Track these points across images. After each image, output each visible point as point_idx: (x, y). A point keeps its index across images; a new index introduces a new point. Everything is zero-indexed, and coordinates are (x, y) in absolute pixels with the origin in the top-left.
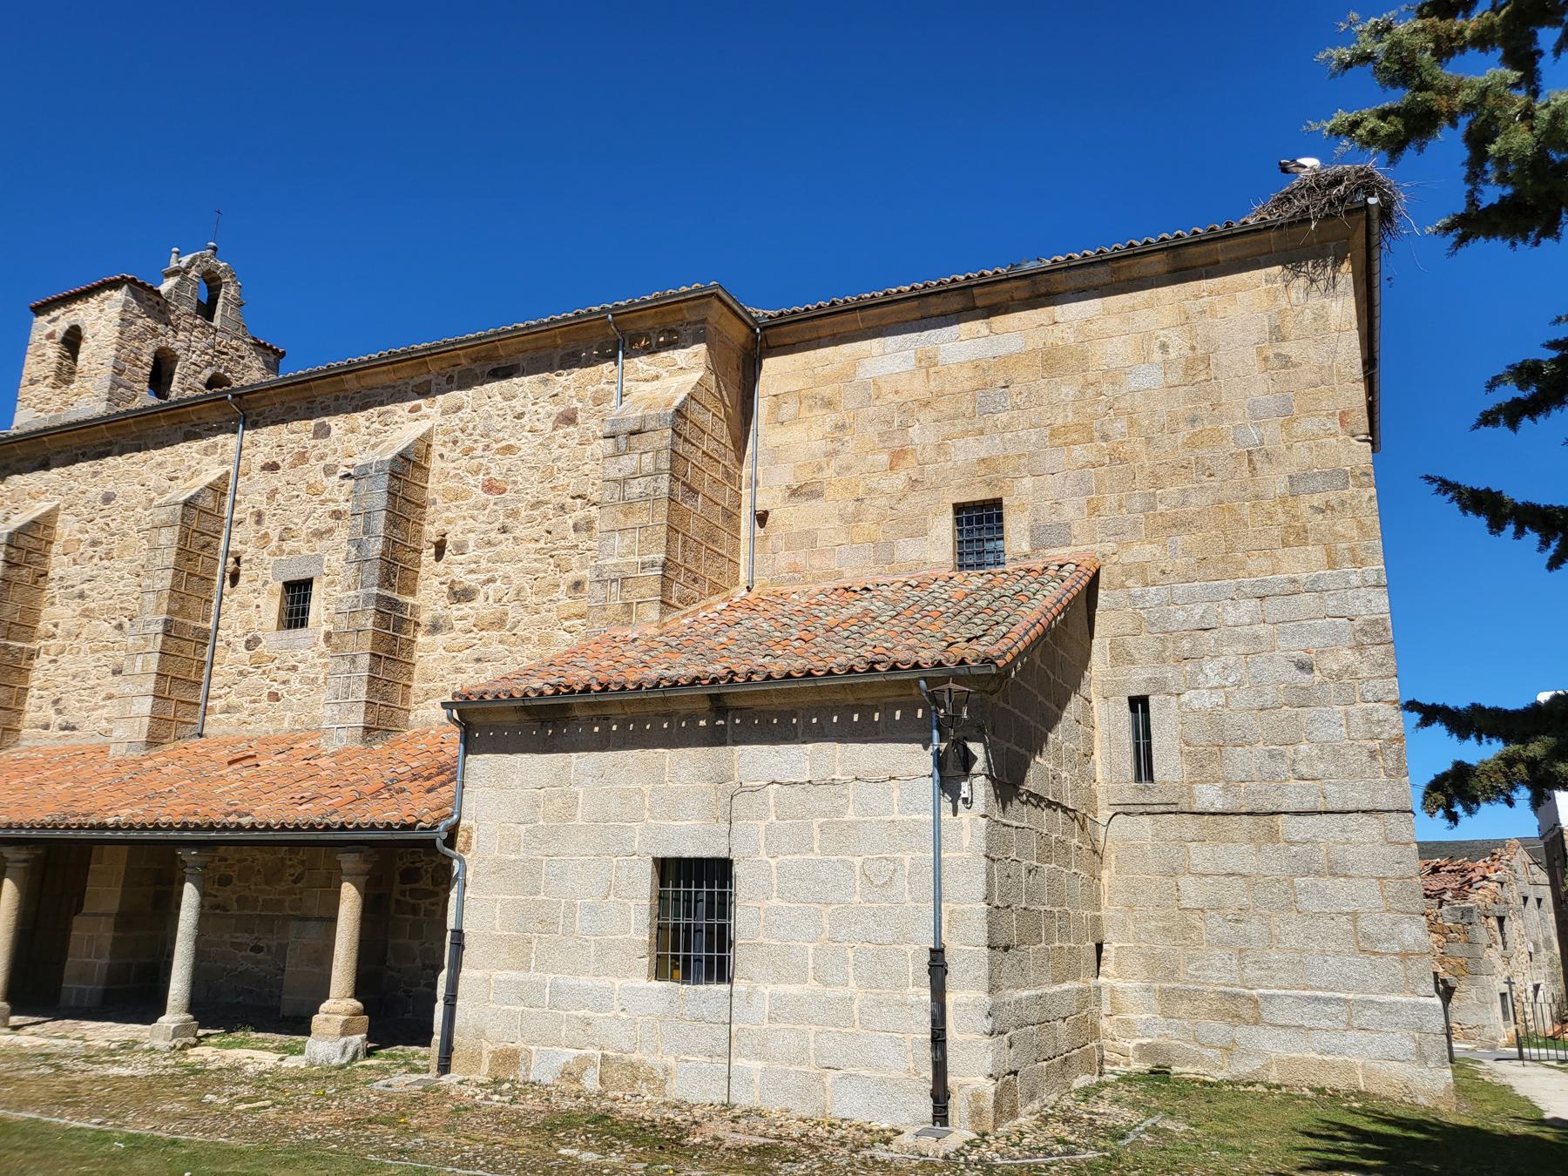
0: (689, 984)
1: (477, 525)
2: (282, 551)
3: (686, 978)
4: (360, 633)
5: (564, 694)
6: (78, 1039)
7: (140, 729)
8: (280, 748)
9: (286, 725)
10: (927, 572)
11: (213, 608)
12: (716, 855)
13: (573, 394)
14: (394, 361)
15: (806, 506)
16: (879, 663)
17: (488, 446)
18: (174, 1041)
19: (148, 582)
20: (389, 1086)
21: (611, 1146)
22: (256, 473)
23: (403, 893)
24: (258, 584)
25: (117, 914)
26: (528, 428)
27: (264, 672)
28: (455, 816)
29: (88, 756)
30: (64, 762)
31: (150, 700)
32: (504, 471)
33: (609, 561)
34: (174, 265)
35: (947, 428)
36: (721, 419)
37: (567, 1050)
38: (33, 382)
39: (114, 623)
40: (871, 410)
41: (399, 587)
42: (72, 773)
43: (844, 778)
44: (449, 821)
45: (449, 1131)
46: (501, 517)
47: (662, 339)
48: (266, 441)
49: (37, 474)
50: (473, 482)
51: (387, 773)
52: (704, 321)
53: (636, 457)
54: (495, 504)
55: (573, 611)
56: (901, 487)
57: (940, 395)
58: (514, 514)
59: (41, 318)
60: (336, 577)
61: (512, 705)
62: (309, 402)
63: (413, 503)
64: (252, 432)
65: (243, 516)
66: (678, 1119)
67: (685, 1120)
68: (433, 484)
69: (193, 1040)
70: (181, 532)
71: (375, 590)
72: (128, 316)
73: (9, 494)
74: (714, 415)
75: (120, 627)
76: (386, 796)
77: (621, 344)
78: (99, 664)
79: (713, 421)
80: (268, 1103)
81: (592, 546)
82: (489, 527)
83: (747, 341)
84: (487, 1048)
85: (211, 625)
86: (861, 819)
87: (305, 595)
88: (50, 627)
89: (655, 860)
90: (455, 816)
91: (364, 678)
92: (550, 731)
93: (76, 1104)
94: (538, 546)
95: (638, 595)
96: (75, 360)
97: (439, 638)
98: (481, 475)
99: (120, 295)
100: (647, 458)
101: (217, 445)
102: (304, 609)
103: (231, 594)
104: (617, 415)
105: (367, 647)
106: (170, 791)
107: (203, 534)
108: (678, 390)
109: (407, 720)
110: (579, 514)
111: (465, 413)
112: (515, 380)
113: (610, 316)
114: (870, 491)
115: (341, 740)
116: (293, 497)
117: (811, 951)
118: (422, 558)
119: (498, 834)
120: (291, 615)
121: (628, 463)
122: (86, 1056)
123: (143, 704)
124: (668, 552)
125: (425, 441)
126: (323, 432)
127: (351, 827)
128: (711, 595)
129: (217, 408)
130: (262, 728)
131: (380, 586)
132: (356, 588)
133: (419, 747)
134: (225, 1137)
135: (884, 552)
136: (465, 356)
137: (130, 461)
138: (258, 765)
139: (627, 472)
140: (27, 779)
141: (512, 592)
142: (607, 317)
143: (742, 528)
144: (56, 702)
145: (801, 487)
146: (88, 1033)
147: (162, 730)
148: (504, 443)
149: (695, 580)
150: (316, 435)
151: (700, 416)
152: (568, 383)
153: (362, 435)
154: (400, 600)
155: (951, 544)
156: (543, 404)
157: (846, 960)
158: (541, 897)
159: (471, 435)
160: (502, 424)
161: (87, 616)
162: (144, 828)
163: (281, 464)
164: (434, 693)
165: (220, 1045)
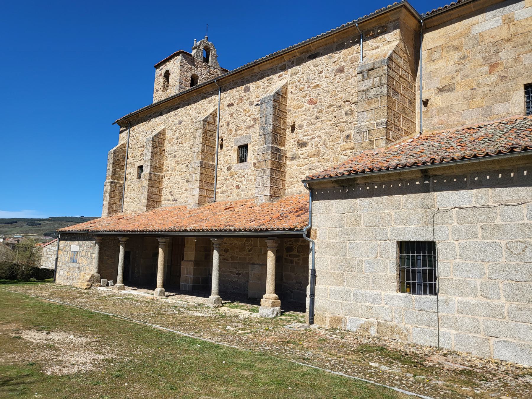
0: (416, 294)
1: (307, 117)
2: (237, 135)
3: (414, 292)
4: (266, 161)
5: (353, 174)
6: (185, 301)
7: (195, 200)
8: (241, 204)
9: (242, 197)
10: (510, 118)
11: (215, 157)
12: (427, 240)
13: (342, 60)
14: (271, 59)
15: (446, 96)
16: (516, 148)
17: (309, 86)
18: (215, 305)
19: (194, 149)
20: (292, 328)
21: (392, 363)
22: (226, 108)
23: (287, 256)
24: (230, 147)
25: (194, 261)
26: (324, 77)
27: (234, 179)
28: (310, 225)
29: (181, 209)
30: (174, 211)
31: (198, 189)
32: (316, 95)
33: (362, 124)
34: (195, 45)
35: (520, 50)
36: (406, 62)
37: (362, 319)
38: (157, 91)
39: (185, 165)
40: (479, 48)
41: (279, 144)
42: (176, 214)
43: (494, 204)
44: (308, 227)
45: (320, 350)
46: (316, 113)
47: (379, 31)
48: (228, 96)
49: (159, 117)
50: (304, 101)
51: (280, 211)
52: (398, 19)
53: (372, 79)
54: (313, 108)
55: (346, 147)
56: (495, 81)
57: (516, 35)
58: (321, 111)
59: (158, 69)
60: (256, 143)
61: (331, 180)
62: (242, 79)
63: (282, 111)
64: (223, 93)
65: (223, 124)
66: (418, 352)
67: (421, 353)
68: (289, 103)
69: (221, 305)
70: (203, 131)
71: (271, 145)
72: (182, 64)
73: (152, 125)
74: (404, 60)
75: (187, 166)
76: (281, 218)
77: (361, 36)
78: (182, 179)
79: (403, 62)
80: (249, 331)
81: (353, 120)
82: (311, 118)
83: (416, 27)
84: (328, 316)
85: (215, 163)
86: (505, 223)
87: (246, 150)
88: (167, 167)
89: (398, 242)
90: (310, 225)
91: (268, 178)
92: (347, 190)
93: (185, 326)
94: (331, 123)
95: (376, 137)
96: (168, 82)
97: (295, 162)
98: (307, 97)
99: (179, 58)
100: (377, 80)
101: (212, 99)
102: (246, 155)
103: (221, 152)
104: (363, 64)
105: (269, 166)
106: (207, 219)
107: (210, 131)
108: (388, 50)
109: (285, 193)
110: (347, 108)
111: (300, 75)
112: (318, 58)
113: (357, 24)
114: (479, 84)
115: (262, 200)
116: (239, 115)
117: (478, 283)
118: (287, 132)
119: (327, 232)
120: (241, 158)
121: (368, 83)
122: (188, 308)
123: (196, 191)
124: (388, 118)
125: (285, 87)
126: (248, 90)
127: (270, 230)
128: (405, 136)
129: (212, 86)
130: (234, 198)
131: (272, 143)
132: (264, 145)
133: (291, 202)
134: (236, 345)
135: (487, 111)
136: (298, 52)
137: (186, 109)
138: (234, 210)
139: (368, 87)
140: (164, 216)
141: (322, 142)
142: (355, 25)
143: (416, 108)
144: (171, 192)
145: (444, 87)
146: (189, 300)
147: (203, 200)
148: (315, 84)
149: (399, 130)
150: (245, 91)
151: (398, 60)
152: (340, 56)
153: (261, 89)
154: (280, 148)
155: (523, 103)
156: (330, 66)
157: (499, 288)
158: (347, 257)
159: (302, 83)
160: (314, 77)
161: (177, 163)
162: (199, 231)
163: (234, 104)
164: (294, 182)
165: (230, 307)
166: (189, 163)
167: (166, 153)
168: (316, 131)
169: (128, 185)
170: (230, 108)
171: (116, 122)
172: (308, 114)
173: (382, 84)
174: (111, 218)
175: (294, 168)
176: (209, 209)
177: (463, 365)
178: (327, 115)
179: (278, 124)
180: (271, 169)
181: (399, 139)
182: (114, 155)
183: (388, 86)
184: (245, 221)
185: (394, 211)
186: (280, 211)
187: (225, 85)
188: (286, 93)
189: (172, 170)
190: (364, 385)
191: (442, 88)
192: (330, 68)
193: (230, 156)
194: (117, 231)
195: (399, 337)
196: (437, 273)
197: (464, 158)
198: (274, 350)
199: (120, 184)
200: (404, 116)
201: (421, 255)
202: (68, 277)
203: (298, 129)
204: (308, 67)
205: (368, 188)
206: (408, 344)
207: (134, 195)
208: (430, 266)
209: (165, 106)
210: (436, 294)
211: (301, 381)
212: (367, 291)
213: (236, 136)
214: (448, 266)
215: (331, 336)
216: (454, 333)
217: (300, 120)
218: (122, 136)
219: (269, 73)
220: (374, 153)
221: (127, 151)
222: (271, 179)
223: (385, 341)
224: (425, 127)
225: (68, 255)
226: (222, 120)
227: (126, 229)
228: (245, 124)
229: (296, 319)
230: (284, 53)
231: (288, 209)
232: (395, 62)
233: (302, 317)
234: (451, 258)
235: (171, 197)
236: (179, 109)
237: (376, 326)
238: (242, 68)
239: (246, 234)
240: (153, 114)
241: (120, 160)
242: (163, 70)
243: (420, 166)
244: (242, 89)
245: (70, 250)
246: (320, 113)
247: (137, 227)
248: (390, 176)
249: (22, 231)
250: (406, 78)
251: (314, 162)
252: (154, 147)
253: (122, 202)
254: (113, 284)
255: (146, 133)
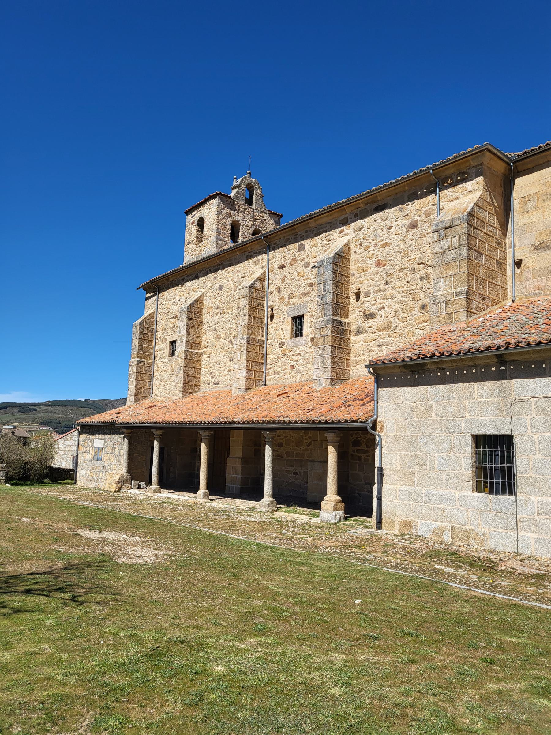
0: (493, 494)
2: (290, 304)
3: (492, 492)
4: (326, 337)
5: (422, 358)
6: (234, 505)
7: (242, 383)
8: (297, 388)
9: (298, 379)
11: (265, 331)
13: (415, 213)
14: (329, 211)
17: (376, 244)
18: (269, 508)
20: (356, 533)
21: (460, 566)
22: (276, 270)
24: (282, 319)
26: (394, 233)
27: (287, 357)
28: (375, 416)
29: (225, 395)
30: (216, 397)
31: (244, 371)
32: (385, 255)
34: (235, 184)
36: (493, 215)
37: (435, 522)
38: (189, 243)
39: (228, 340)
41: (341, 315)
44: (373, 419)
45: (383, 553)
46: (385, 278)
47: (459, 178)
49: (194, 281)
50: (370, 263)
52: (481, 164)
53: (449, 240)
54: (382, 272)
55: (422, 319)
58: (391, 275)
59: (189, 216)
60: (313, 313)
63: (344, 276)
64: (273, 252)
65: (273, 290)
67: (496, 558)
68: (352, 266)
69: (275, 509)
71: (331, 317)
72: (220, 209)
74: (489, 213)
75: (230, 341)
76: (344, 408)
77: (438, 184)
81: (430, 287)
82: (380, 283)
84: (397, 519)
85: (264, 338)
87: (301, 322)
88: (206, 343)
89: (473, 436)
90: (375, 416)
92: (417, 376)
93: (237, 530)
94: (403, 289)
95: (455, 309)
96: (203, 232)
97: (361, 337)
98: (374, 258)
99: (216, 201)
100: (455, 240)
101: (259, 260)
102: (301, 328)
104: (438, 220)
105: (330, 343)
106: (256, 408)
107: (258, 299)
108: (469, 203)
109: (349, 374)
110: (423, 272)
111: (365, 230)
112: (387, 211)
113: (431, 171)
116: (292, 279)
118: (350, 301)
119: (395, 424)
120: (296, 331)
121: (445, 244)
122: (238, 512)
124: (469, 286)
125: (347, 246)
128: (492, 305)
129: (258, 243)
130: (288, 381)
131: (333, 315)
133: (356, 386)
136: (362, 202)
137: (227, 271)
138: (289, 396)
139: (445, 248)
140: (205, 404)
141: (393, 313)
142: (430, 171)
143: (508, 270)
144: (211, 373)
145: (540, 244)
148: (384, 242)
149: (484, 299)
150: (299, 250)
151: (482, 215)
152: (412, 208)
154: (342, 320)
156: (401, 220)
158: (418, 453)
159: (368, 240)
161: (218, 338)
162: (248, 423)
163: (286, 265)
164: (360, 362)
165: (286, 512)
166: (232, 338)
167: (205, 326)
168: (385, 300)
169: (157, 364)
170: (281, 270)
171: (141, 287)
172: (376, 279)
173: (461, 246)
174: (139, 406)
175: (360, 344)
176: (258, 395)
177: (539, 570)
178: (398, 280)
179: (339, 291)
180: (332, 346)
181: (484, 310)
182: (140, 328)
183: (469, 247)
184: (301, 410)
185: (468, 401)
186: (343, 398)
187: (274, 242)
188: (349, 254)
189: (213, 346)
190: (419, 580)
191: (538, 245)
192: (401, 222)
193: (282, 329)
194: (151, 423)
195: (475, 543)
196: (515, 470)
197: (540, 343)
198: (333, 552)
199: (148, 363)
200: (491, 281)
201: (499, 450)
202: (92, 477)
203: (364, 297)
204: (375, 221)
205: (439, 374)
206: (484, 550)
207: (165, 376)
208: (509, 462)
209: (201, 268)
210: (515, 494)
211: (356, 576)
212: (441, 491)
213: (290, 305)
214: (527, 462)
215: (399, 541)
216: (534, 537)
217: (367, 286)
218: (148, 304)
219: (327, 228)
220: (452, 329)
221: (155, 322)
222: (332, 359)
223: (459, 546)
224: (519, 293)
225: (91, 452)
226: (272, 285)
227: (161, 421)
228: (300, 290)
229: (362, 524)
230: (345, 204)
231: (352, 396)
232: (477, 218)
233: (370, 522)
234: (530, 454)
235: (211, 379)
236: (219, 271)
237: (450, 530)
238: (294, 222)
239: (302, 427)
240: (187, 277)
241: (147, 334)
242: (195, 217)
243: (493, 351)
244: (296, 247)
245: (93, 446)
246: (390, 278)
247: (175, 417)
248: (462, 361)
249: (13, 420)
250: (493, 234)
251: (384, 338)
252: (189, 319)
253: (151, 385)
254: (145, 487)
255: (179, 301)
